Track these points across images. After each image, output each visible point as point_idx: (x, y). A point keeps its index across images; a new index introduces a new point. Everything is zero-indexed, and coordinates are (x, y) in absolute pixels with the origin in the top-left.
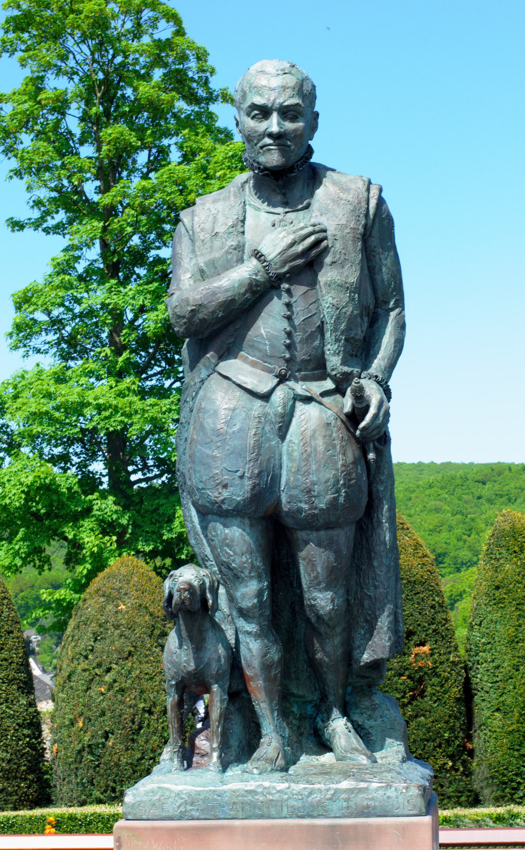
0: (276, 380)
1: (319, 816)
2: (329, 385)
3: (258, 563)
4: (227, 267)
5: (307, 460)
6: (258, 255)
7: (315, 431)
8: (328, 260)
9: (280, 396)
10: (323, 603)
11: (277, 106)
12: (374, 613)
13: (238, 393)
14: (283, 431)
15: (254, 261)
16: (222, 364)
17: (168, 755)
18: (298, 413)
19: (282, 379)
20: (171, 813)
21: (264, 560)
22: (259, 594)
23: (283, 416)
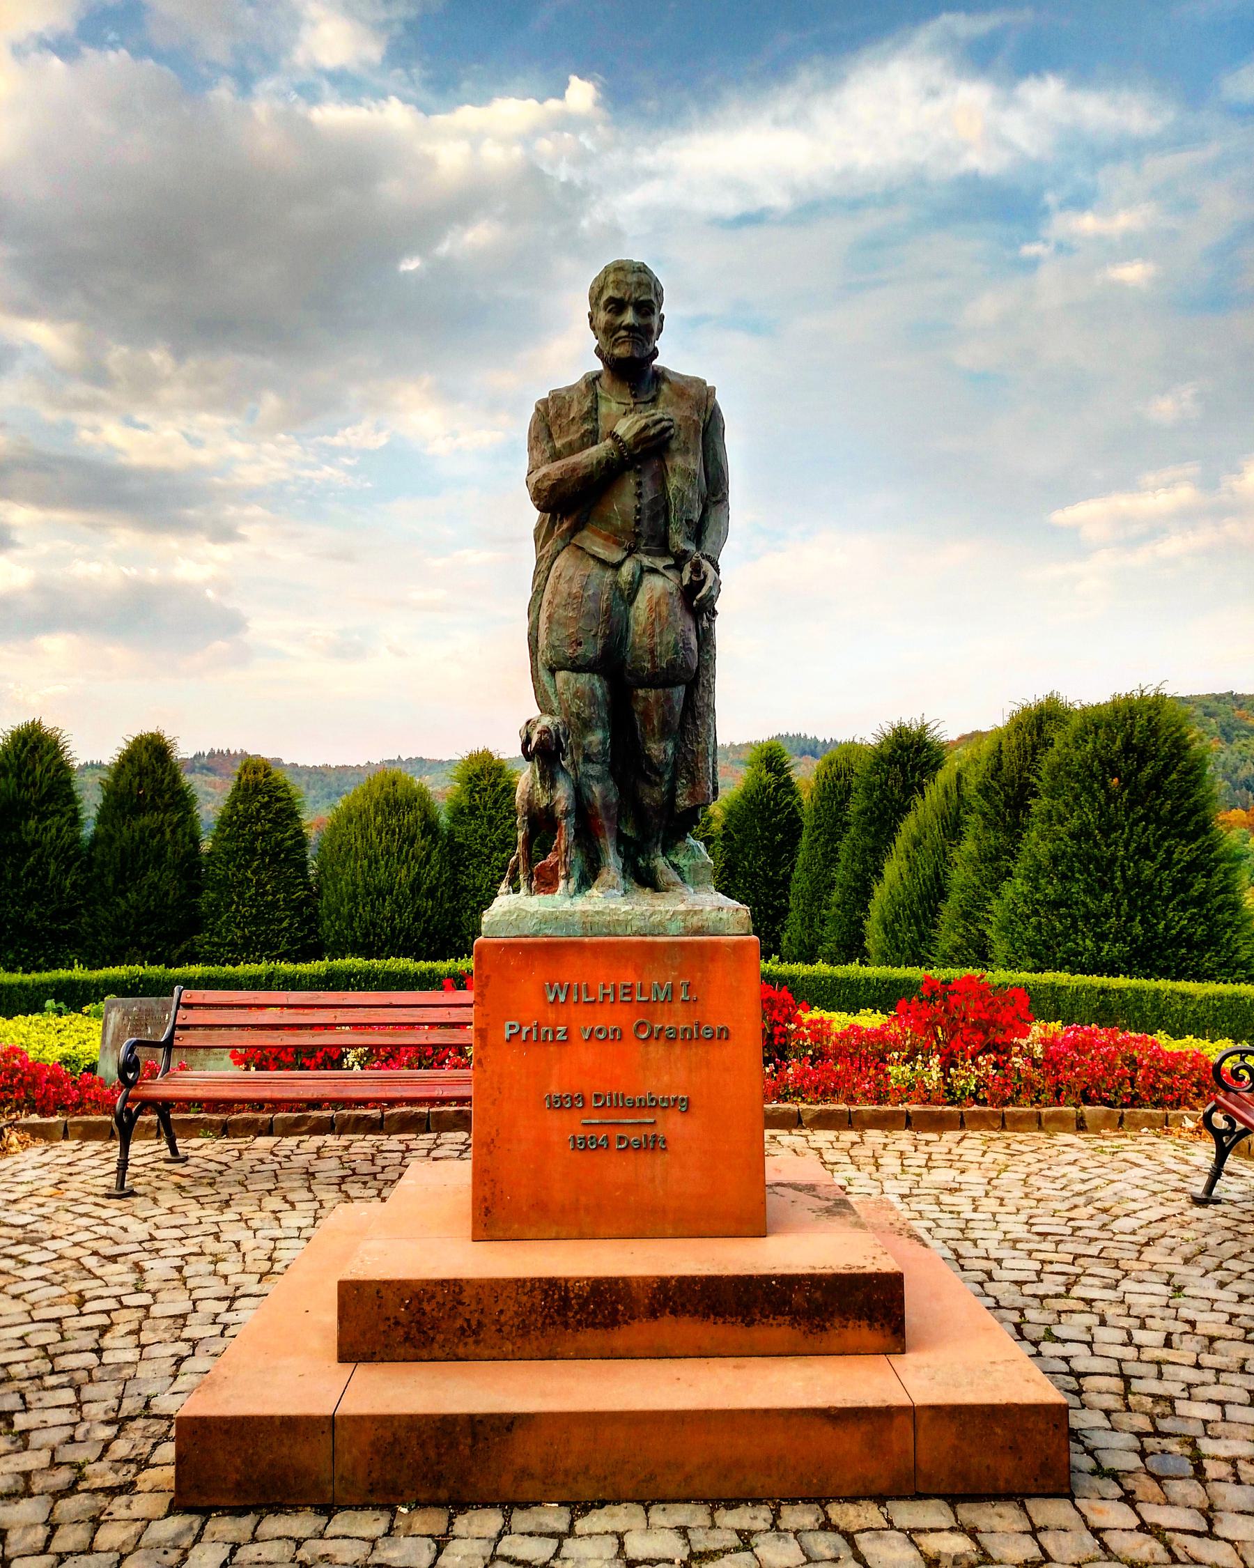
0: (625, 553)
1: (659, 935)
2: (671, 562)
3: (603, 715)
4: (583, 446)
5: (652, 624)
6: (613, 436)
7: (659, 598)
8: (674, 445)
9: (627, 570)
10: (656, 753)
11: (633, 300)
12: (696, 764)
13: (592, 562)
14: (630, 599)
15: (609, 442)
16: (578, 537)
17: (503, 887)
18: (645, 582)
19: (631, 552)
20: (526, 932)
21: (608, 713)
22: (603, 743)
23: (631, 583)
